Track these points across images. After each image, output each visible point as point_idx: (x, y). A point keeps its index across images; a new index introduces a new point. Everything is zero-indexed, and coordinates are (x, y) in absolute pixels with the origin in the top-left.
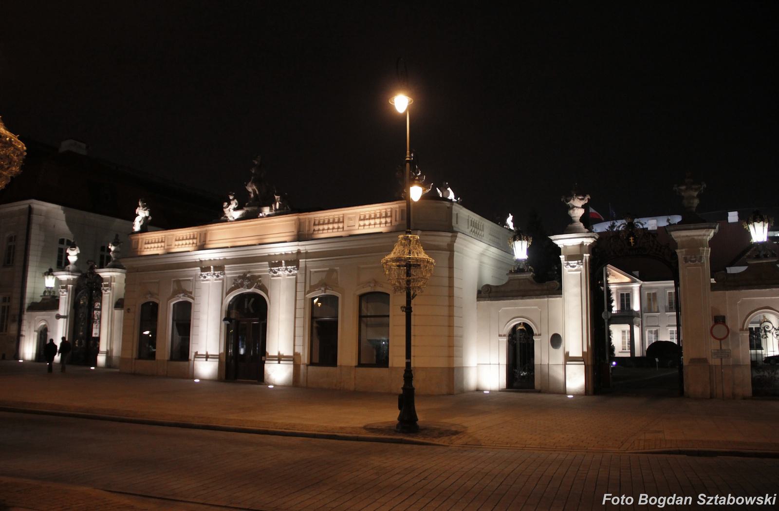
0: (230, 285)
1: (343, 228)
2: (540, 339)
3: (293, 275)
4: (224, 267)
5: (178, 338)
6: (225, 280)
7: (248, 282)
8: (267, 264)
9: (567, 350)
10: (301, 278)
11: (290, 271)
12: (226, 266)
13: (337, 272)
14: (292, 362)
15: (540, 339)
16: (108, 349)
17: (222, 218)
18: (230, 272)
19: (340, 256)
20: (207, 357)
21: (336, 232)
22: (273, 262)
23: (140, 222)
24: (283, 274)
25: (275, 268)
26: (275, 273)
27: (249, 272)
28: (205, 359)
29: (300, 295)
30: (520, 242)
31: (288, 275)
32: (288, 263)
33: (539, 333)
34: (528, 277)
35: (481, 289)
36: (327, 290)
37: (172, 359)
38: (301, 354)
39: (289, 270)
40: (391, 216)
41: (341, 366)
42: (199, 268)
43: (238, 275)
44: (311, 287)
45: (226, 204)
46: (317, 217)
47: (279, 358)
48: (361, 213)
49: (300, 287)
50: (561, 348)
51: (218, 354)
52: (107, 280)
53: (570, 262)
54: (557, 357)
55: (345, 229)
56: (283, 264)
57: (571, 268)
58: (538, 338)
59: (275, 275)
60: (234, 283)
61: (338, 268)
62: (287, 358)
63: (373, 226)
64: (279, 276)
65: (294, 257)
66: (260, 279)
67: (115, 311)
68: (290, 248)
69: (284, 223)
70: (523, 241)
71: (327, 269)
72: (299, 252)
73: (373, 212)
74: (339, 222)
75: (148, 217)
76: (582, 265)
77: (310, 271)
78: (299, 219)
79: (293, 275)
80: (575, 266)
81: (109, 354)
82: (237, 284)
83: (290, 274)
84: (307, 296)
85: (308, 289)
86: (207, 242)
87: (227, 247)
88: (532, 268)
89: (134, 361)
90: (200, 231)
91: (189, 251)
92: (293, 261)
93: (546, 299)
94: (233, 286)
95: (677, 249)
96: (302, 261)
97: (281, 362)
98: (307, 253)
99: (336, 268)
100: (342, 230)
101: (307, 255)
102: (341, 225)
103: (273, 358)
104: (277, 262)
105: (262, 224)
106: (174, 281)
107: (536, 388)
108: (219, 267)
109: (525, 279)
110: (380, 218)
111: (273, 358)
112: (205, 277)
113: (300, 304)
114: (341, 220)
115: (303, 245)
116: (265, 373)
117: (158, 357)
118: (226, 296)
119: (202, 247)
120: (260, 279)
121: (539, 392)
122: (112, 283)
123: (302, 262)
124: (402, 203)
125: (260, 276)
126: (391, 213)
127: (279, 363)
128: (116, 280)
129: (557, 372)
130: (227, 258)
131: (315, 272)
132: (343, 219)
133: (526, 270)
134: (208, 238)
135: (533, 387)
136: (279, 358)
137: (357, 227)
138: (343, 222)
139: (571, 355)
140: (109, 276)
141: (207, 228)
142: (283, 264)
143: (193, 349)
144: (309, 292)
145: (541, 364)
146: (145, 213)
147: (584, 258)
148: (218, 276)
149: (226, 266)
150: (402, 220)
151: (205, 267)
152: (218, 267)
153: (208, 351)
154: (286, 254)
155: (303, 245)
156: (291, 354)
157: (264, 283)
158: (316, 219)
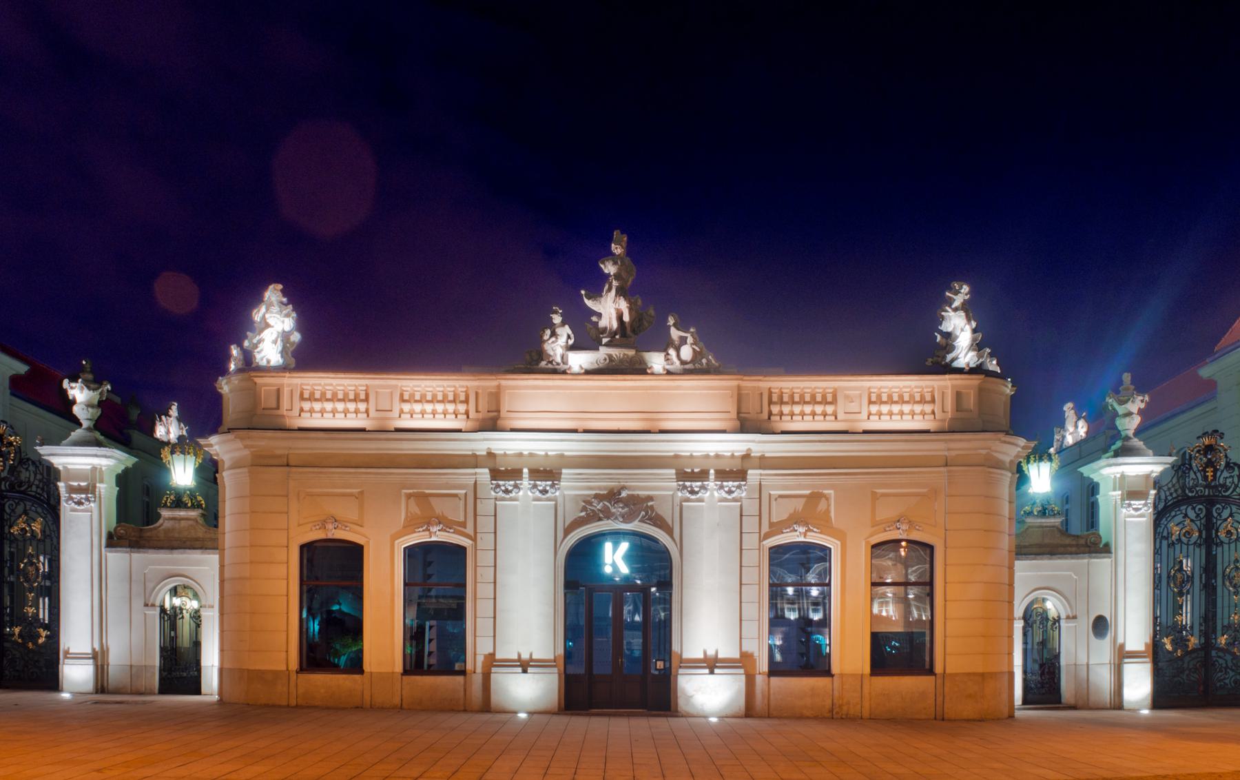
0: (573, 513)
1: (367, 411)
2: (1074, 625)
3: (735, 500)
4: (561, 474)
5: (193, 625)
6: (560, 501)
7: (623, 508)
8: (671, 474)
9: (1120, 640)
10: (751, 507)
11: (544, 492)
12: (564, 471)
13: (827, 499)
14: (91, 661)
15: (1074, 625)
16: (97, 647)
17: (543, 364)
18: (572, 486)
19: (834, 468)
20: (525, 665)
21: (353, 419)
22: (689, 470)
23: (275, 342)
24: (712, 491)
25: (694, 484)
26: (693, 492)
27: (624, 488)
28: (520, 670)
29: (751, 541)
30: (1035, 464)
31: (725, 500)
32: (723, 475)
33: (1074, 614)
34: (1057, 524)
35: (112, 530)
36: (809, 533)
37: (406, 672)
38: (756, 654)
39: (726, 489)
40: (466, 401)
41: (842, 675)
42: (487, 471)
43: (594, 492)
44: (771, 525)
45: (548, 332)
46: (308, 385)
47: (712, 664)
48: (872, 390)
49: (750, 524)
50: (1108, 638)
51: (552, 657)
52: (78, 475)
53: (1132, 502)
54: (1102, 652)
55: (839, 418)
56: (712, 476)
57: (1133, 512)
58: (1074, 623)
59: (693, 497)
60: (584, 509)
61: (832, 492)
62: (729, 664)
63: (309, 414)
64: (701, 500)
65: (736, 465)
66: (650, 504)
67: (108, 554)
68: (734, 445)
69: (722, 392)
70: (188, 456)
71: (807, 492)
72: (746, 456)
73: (353, 388)
74: (824, 402)
75: (290, 333)
76: (95, 501)
77: (770, 495)
78: (739, 388)
79: (735, 500)
80: (1140, 509)
81: (99, 658)
82: (593, 511)
83: (729, 497)
84: (764, 543)
85: (765, 528)
86: (503, 414)
87: (575, 431)
88: (203, 502)
89: (293, 676)
90: (478, 387)
91: (459, 431)
92: (734, 472)
93: (1086, 561)
94: (583, 514)
95: (60, 481)
96: (753, 475)
97: (716, 671)
98: (762, 458)
99: (826, 492)
100: (833, 418)
101: (765, 463)
102: (830, 409)
103: (694, 664)
104: (696, 470)
105: (651, 388)
106: (409, 496)
107: (1063, 701)
108: (547, 473)
109: (1053, 527)
110: (355, 400)
111: (694, 664)
112: (507, 491)
113: (751, 557)
114: (829, 398)
115: (760, 442)
116: (679, 694)
117: (369, 663)
118: (564, 538)
119: (492, 424)
120: (650, 504)
121: (1073, 707)
122: (98, 485)
123: (566, 474)
124: (962, 379)
125: (650, 498)
126: (367, 395)
127: (712, 672)
128: (106, 478)
129: (1103, 678)
130: (566, 453)
131: (781, 496)
132: (367, 395)
133: (189, 505)
134: (505, 407)
135: (1060, 702)
136: (712, 664)
137: (396, 413)
138: (367, 400)
139: (1128, 648)
140: (89, 467)
141: (503, 383)
142: (712, 476)
143: (478, 646)
144: (767, 536)
145: (1075, 665)
146: (283, 322)
147: (97, 490)
148: (730, 492)
149: (564, 471)
150: (957, 411)
151: (506, 470)
152: (545, 471)
153: (520, 651)
154: (717, 456)
155: (760, 442)
156: (737, 656)
157: (660, 512)
158: (305, 387)
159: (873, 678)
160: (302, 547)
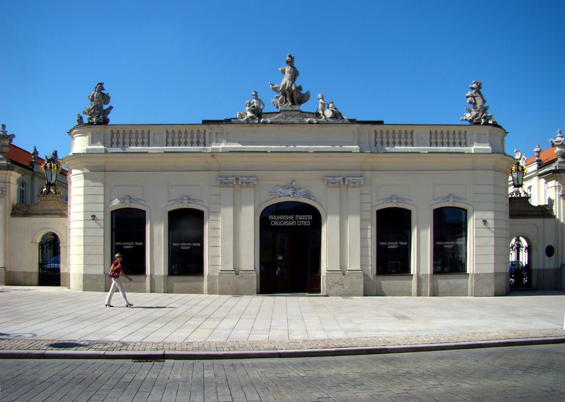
159: (169, 277)
160: (145, 211)
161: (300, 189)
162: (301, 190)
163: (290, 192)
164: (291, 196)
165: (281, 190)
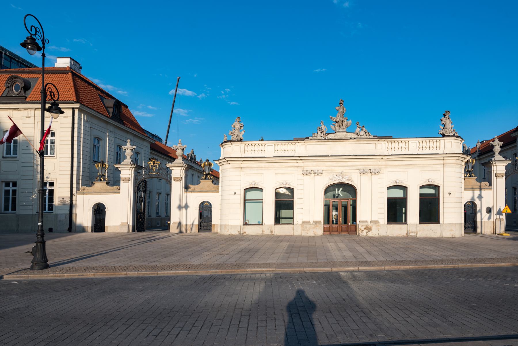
161: (346, 175)
162: (346, 176)
163: (341, 177)
164: (341, 179)
165: (336, 176)
